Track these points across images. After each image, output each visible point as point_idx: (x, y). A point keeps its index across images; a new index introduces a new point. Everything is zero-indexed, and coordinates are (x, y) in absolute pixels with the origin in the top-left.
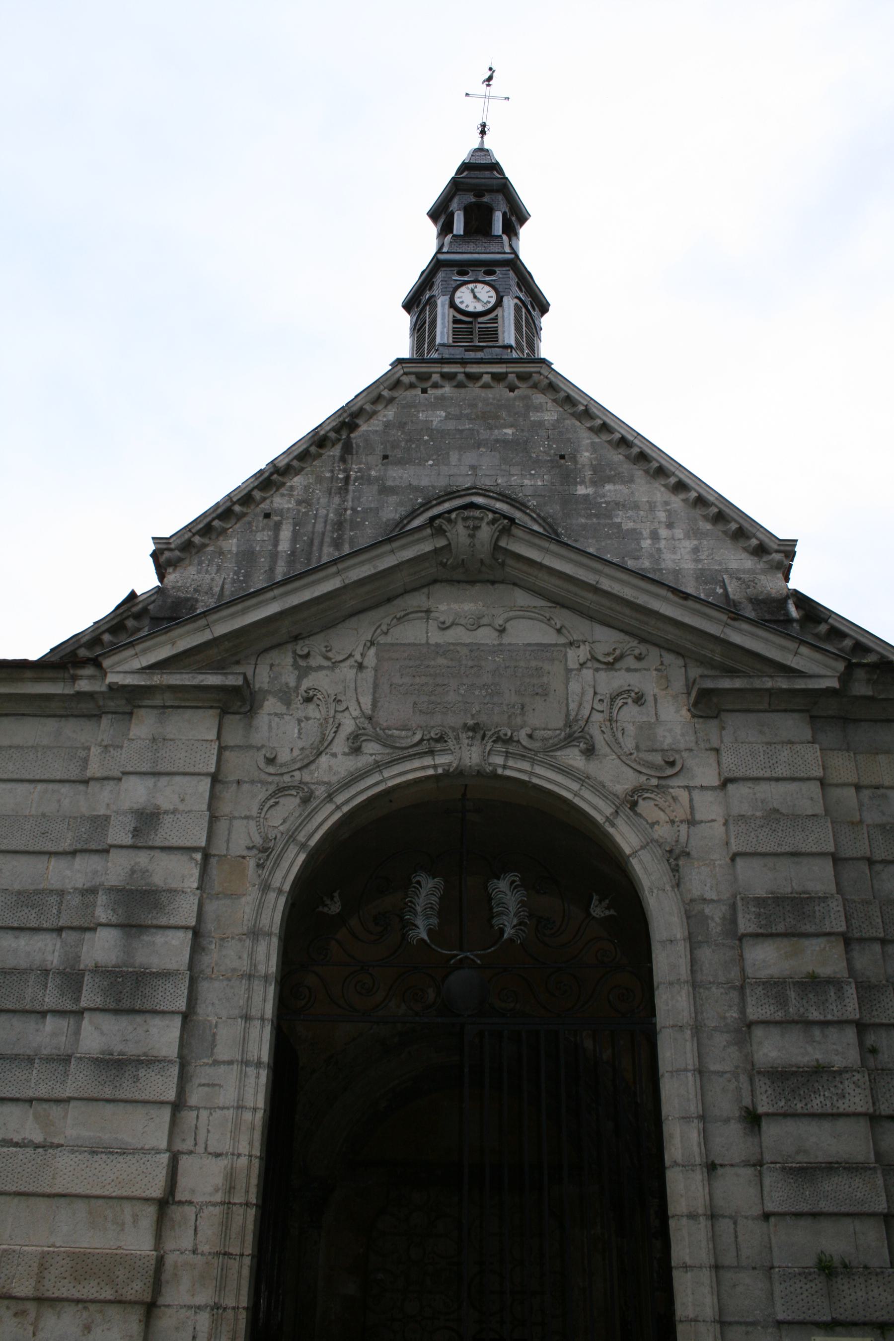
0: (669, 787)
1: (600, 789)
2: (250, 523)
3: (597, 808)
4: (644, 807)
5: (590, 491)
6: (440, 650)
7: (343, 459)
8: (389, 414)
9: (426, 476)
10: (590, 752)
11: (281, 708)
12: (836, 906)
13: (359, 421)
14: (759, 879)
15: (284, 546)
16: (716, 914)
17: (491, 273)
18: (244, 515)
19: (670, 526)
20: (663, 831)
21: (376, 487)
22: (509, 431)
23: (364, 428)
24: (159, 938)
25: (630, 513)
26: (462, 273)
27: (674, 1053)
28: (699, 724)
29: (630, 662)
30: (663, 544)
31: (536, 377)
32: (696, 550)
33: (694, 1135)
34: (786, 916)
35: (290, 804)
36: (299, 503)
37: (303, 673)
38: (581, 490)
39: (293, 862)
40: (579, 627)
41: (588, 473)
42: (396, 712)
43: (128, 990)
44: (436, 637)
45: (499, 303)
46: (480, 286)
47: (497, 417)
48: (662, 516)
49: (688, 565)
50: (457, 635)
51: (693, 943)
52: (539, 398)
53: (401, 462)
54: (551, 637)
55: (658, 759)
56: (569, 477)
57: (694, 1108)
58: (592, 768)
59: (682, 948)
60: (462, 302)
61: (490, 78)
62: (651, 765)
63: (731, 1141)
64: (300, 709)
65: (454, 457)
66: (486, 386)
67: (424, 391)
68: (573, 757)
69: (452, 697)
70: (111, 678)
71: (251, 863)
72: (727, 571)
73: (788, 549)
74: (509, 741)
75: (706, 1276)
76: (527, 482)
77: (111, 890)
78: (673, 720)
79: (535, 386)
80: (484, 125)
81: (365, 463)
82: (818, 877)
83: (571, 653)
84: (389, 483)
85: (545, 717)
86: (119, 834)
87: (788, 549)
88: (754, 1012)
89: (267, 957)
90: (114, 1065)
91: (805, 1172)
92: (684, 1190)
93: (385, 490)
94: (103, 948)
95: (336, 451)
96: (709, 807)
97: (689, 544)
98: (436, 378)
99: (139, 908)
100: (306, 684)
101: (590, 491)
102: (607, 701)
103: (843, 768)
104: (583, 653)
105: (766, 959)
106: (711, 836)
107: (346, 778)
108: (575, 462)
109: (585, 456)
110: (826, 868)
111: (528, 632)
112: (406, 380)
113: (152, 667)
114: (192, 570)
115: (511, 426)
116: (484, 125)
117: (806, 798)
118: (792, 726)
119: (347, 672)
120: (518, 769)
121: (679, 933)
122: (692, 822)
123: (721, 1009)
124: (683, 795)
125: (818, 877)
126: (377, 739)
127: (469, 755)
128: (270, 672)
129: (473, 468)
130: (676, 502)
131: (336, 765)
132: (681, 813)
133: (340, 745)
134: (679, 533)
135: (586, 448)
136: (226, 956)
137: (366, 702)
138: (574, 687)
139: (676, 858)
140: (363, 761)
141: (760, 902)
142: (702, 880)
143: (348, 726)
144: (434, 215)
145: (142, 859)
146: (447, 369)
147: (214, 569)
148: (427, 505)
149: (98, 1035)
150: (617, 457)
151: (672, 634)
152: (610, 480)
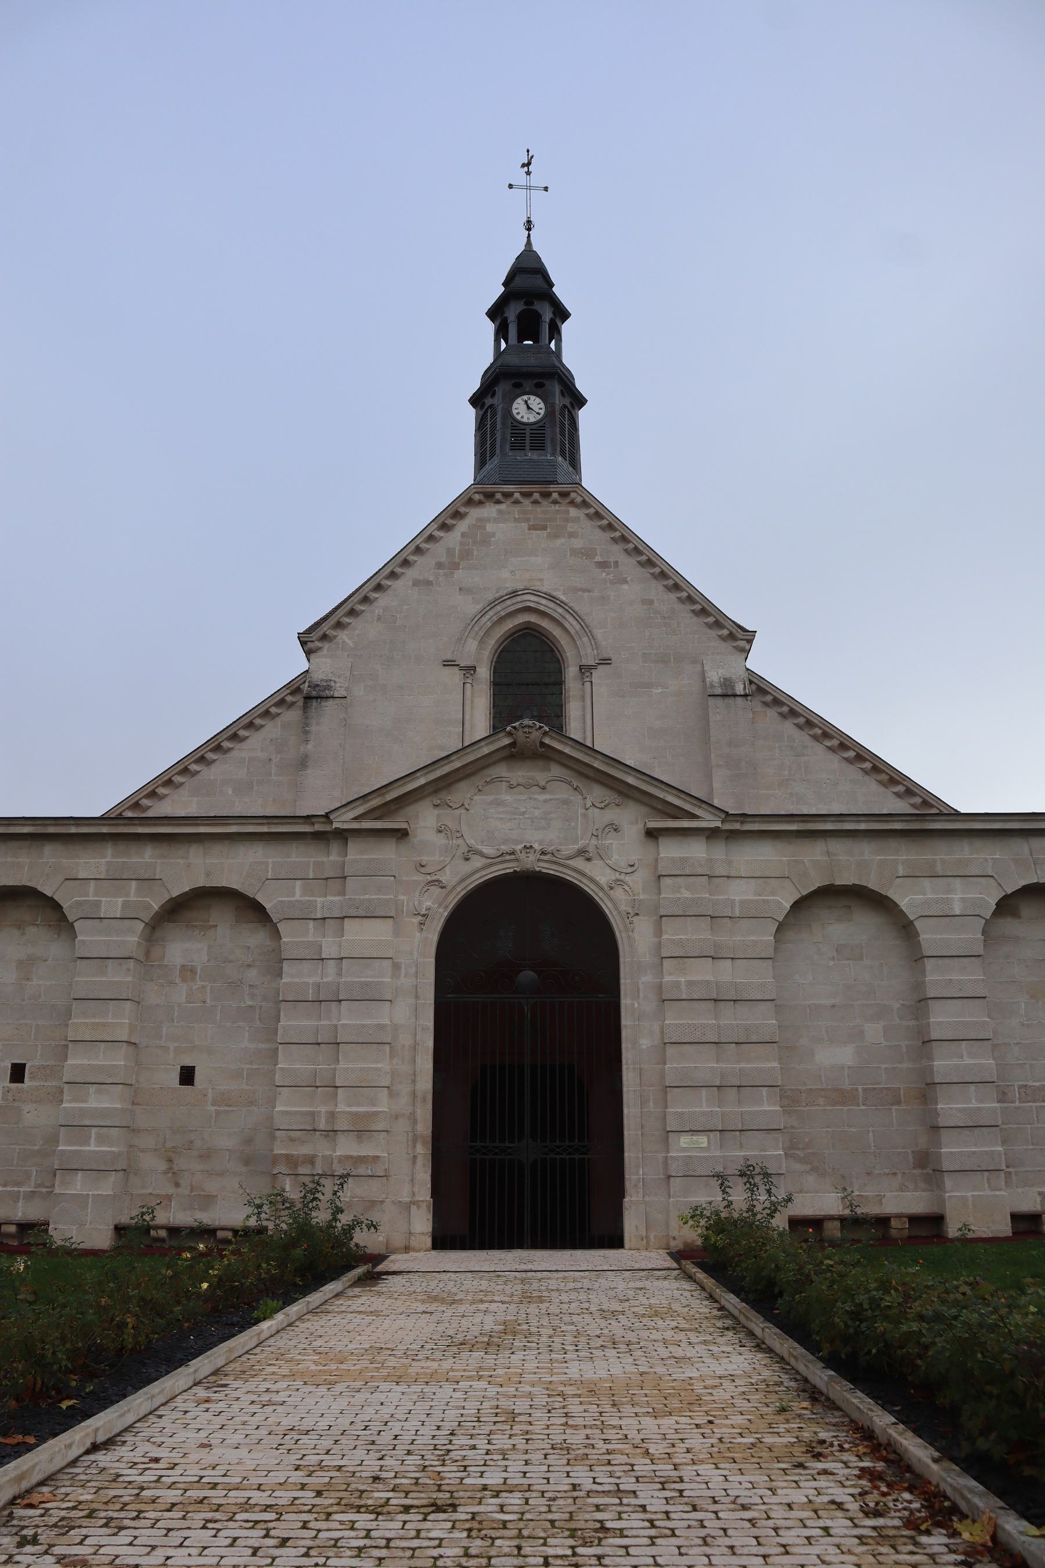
0: (965, 1553)
31: (573, 495)
46: (533, 397)
60: (518, 413)
61: (529, 164)
79: (572, 503)
80: (529, 222)
102: (600, 830)
112: (477, 497)
113: (355, 818)
116: (529, 222)
144: (493, 313)
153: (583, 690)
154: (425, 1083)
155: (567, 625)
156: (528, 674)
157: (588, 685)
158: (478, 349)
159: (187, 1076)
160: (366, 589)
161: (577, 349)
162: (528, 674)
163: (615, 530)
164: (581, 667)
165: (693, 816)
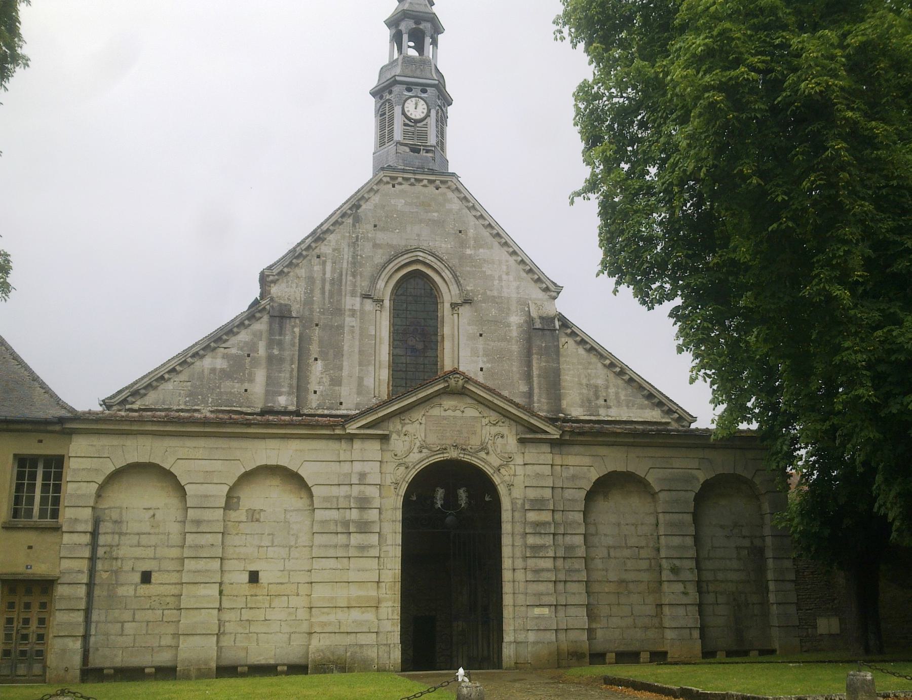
1: (490, 465)
2: (310, 260)
3: (489, 471)
4: (502, 471)
5: (472, 252)
6: (444, 418)
7: (354, 225)
8: (376, 199)
9: (397, 239)
10: (487, 453)
11: (397, 437)
12: (551, 502)
13: (362, 203)
14: (532, 494)
15: (328, 275)
16: (520, 502)
17: (424, 91)
18: (307, 255)
19: (507, 274)
20: (507, 478)
21: (371, 244)
22: (435, 214)
23: (364, 207)
24: (370, 511)
25: (490, 266)
26: (409, 90)
27: (506, 540)
28: (519, 445)
29: (500, 423)
30: (504, 283)
31: (450, 183)
32: (518, 288)
33: (510, 561)
34: (538, 505)
35: (402, 469)
36: (334, 250)
37: (404, 425)
38: (468, 252)
39: (404, 487)
40: (487, 412)
41: (472, 242)
42: (432, 439)
43: (364, 527)
44: (443, 414)
45: (428, 115)
47: (430, 205)
48: (504, 267)
49: (514, 296)
50: (449, 413)
51: (513, 511)
52: (450, 195)
53: (384, 229)
54: (477, 414)
55: (506, 455)
56: (463, 244)
57: (511, 555)
58: (488, 458)
59: (510, 512)
62: (504, 457)
63: (519, 563)
64: (403, 438)
65: (409, 229)
66: (425, 186)
67: (394, 186)
68: (482, 454)
69: (448, 434)
70: (348, 431)
71: (392, 488)
72: (530, 299)
73: (558, 289)
74: (464, 450)
75: (511, 596)
76: (443, 245)
77: (354, 498)
78: (511, 442)
79: (449, 188)
81: (366, 228)
82: (547, 493)
83: (483, 420)
84: (378, 242)
85: (475, 442)
86: (355, 480)
87: (558, 289)
88: (527, 531)
89: (399, 515)
90: (362, 548)
91: (537, 571)
92: (507, 575)
93: (376, 246)
94: (354, 515)
95: (350, 221)
96: (520, 471)
97: (515, 284)
98: (400, 180)
99: (363, 504)
100: (404, 429)
101: (472, 252)
103: (558, 460)
104: (487, 420)
105: (532, 516)
106: (519, 481)
107: (418, 460)
108: (466, 235)
109: (471, 232)
110: (550, 490)
111: (471, 412)
112: (385, 179)
114: (284, 285)
115: (437, 211)
117: (547, 470)
118: (546, 448)
119: (416, 425)
120: (467, 458)
121: (510, 508)
122: (515, 475)
123: (519, 528)
124: (513, 467)
125: (547, 493)
126: (427, 448)
127: (453, 454)
128: (395, 426)
129: (418, 235)
130: (512, 260)
131: (415, 457)
132: (512, 473)
133: (416, 450)
134: (511, 278)
135: (473, 228)
136: (387, 515)
137: (423, 435)
138: (484, 432)
139: (510, 486)
140: (423, 455)
141: (532, 500)
142: (517, 493)
143: (418, 444)
145: (362, 487)
146: (406, 176)
147: (294, 285)
148: (396, 257)
149: (355, 539)
150: (486, 233)
151: (513, 417)
152: (481, 246)
153: (454, 320)
154: (398, 572)
155: (443, 274)
156: (416, 305)
157: (456, 316)
158: (377, 51)
159: (254, 577)
160: (308, 241)
161: (449, 56)
162: (416, 305)
163: (476, 209)
164: (451, 304)
165: (546, 432)
